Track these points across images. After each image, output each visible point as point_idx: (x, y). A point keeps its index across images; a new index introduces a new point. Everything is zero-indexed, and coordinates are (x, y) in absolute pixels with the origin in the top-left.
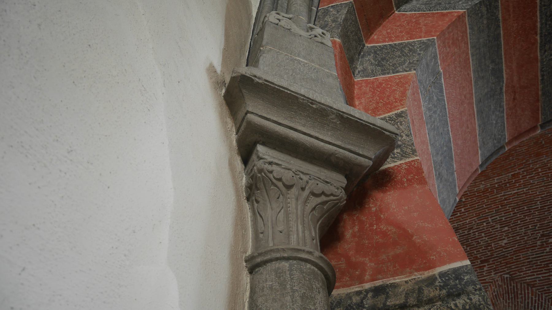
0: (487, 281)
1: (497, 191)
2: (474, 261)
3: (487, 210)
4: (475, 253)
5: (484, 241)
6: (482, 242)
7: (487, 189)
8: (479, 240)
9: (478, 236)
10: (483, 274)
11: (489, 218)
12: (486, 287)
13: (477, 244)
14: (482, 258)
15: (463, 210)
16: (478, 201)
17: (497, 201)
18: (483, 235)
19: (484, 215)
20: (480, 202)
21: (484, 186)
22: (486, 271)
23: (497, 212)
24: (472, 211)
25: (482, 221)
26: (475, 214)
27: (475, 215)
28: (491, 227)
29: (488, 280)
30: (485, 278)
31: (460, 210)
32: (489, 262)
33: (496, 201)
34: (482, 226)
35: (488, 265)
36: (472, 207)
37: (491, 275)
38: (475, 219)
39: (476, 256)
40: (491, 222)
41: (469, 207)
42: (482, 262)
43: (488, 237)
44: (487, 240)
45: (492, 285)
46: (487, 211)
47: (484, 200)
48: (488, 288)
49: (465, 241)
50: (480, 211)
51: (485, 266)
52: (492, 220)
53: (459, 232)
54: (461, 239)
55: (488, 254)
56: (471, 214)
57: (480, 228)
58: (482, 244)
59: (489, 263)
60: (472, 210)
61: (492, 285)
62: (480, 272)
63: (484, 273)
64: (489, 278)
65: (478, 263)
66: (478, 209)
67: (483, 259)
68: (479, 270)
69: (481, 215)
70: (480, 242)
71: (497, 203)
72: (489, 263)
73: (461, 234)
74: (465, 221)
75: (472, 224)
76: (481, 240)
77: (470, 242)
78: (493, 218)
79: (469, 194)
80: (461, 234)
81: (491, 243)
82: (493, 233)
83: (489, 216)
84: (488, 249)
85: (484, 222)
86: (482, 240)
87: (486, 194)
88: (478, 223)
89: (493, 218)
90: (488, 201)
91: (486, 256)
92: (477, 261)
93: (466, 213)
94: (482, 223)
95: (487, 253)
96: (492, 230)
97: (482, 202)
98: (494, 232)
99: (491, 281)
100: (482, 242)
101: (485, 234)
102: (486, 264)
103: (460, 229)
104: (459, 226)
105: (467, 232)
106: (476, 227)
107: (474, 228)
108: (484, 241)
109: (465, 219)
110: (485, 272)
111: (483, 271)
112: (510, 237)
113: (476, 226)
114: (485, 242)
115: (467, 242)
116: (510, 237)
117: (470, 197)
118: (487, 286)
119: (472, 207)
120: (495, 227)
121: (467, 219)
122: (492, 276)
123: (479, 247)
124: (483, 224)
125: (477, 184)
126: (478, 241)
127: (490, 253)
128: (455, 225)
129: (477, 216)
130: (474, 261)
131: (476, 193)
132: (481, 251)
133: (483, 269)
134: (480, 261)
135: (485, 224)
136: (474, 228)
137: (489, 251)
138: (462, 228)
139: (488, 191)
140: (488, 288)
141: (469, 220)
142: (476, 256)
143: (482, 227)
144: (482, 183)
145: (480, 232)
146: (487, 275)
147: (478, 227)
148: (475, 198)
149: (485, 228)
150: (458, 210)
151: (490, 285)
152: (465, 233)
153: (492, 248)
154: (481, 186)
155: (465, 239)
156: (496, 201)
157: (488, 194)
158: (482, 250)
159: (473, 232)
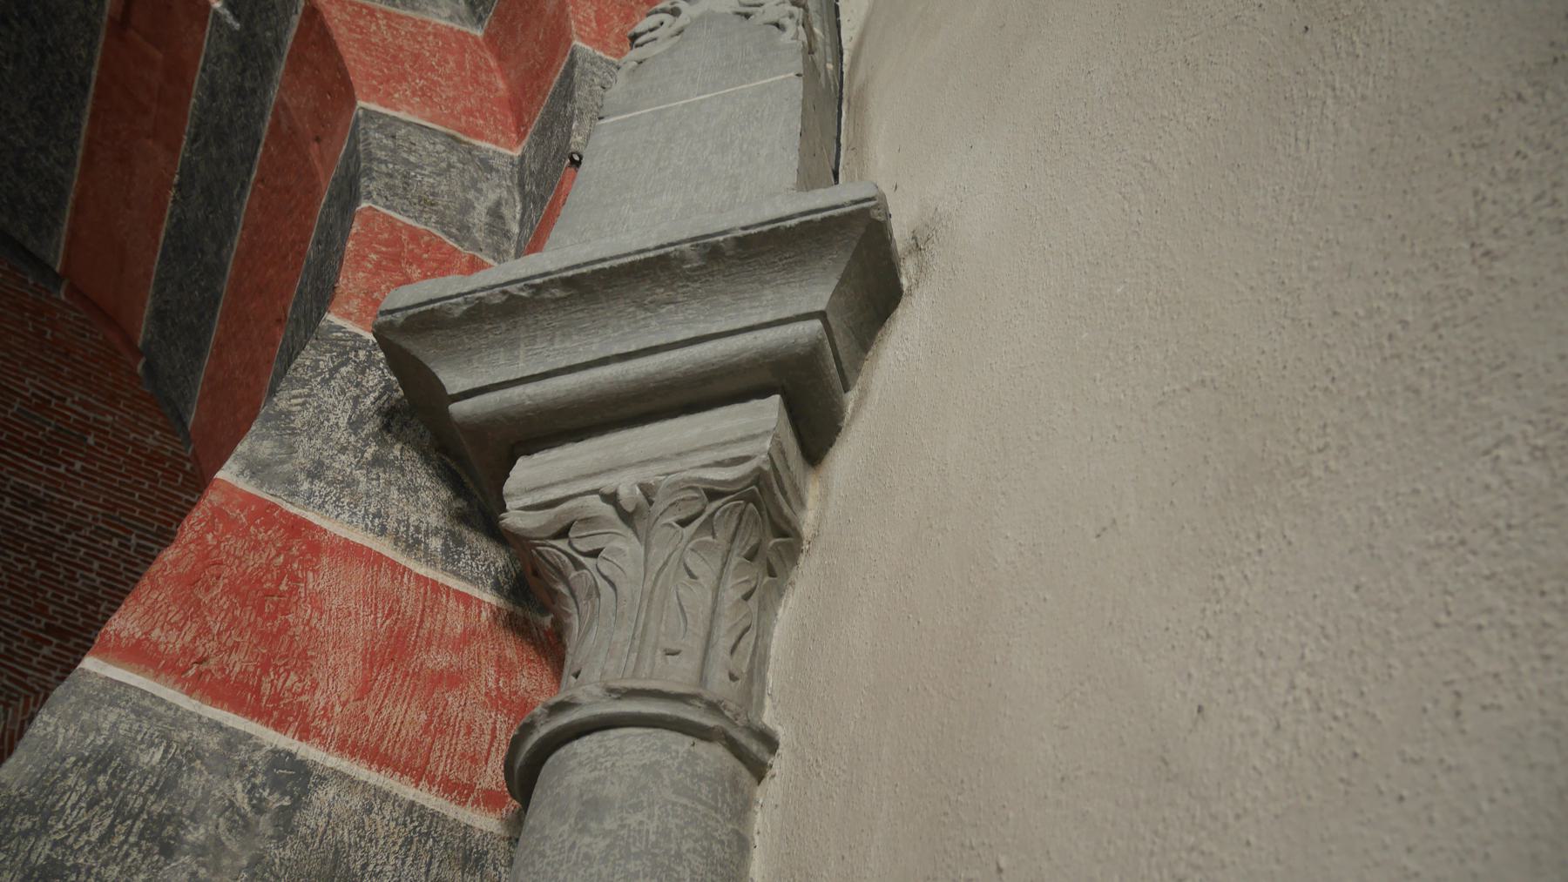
0: (28, 682)
1: (186, 483)
2: (32, 615)
3: (138, 510)
4: (49, 596)
5: (88, 582)
6: (81, 581)
7: (162, 459)
8: (80, 572)
9: (81, 559)
10: (31, 660)
11: (133, 537)
12: (16, 695)
13: (65, 577)
14: (56, 619)
15: (78, 465)
16: (126, 470)
17: (174, 508)
18: (96, 565)
19: (123, 519)
20: (129, 478)
21: (157, 443)
22: (44, 657)
23: (159, 533)
24: (100, 487)
25: (113, 530)
26: (105, 500)
27: (101, 501)
28: (125, 561)
29: (33, 682)
30: (30, 672)
31: (72, 460)
32: (68, 641)
33: (170, 506)
34: (107, 542)
35: (58, 646)
36: (106, 477)
37: (49, 674)
38: (96, 512)
39: (45, 603)
40: (132, 549)
41: (96, 469)
42: (49, 629)
43: (104, 580)
44: (97, 584)
45: (32, 700)
46: (137, 515)
47: (142, 480)
48: (17, 700)
49: (42, 549)
50: (119, 502)
51: (49, 643)
52: (139, 545)
53: (40, 515)
54: (36, 536)
55: (77, 620)
56: (96, 493)
57: (97, 542)
58: (78, 585)
59: (63, 643)
60: (102, 484)
61: (32, 700)
62: (26, 650)
63: (35, 659)
64: (39, 678)
65: (37, 626)
66: (118, 494)
67: (58, 623)
68: (29, 643)
69: (117, 514)
70: (78, 576)
71: (171, 513)
72: (63, 643)
73: (41, 522)
74: (69, 499)
75: (84, 519)
76: (83, 576)
77: (54, 560)
78: (143, 542)
79: (110, 437)
80: (41, 522)
81: (103, 599)
82: (122, 578)
83: (136, 531)
84: (86, 608)
85: (117, 536)
86: (87, 578)
87: (156, 471)
88: (100, 528)
89: (143, 542)
90: (152, 490)
91: (71, 621)
92: (39, 617)
93: (83, 481)
94: (108, 535)
95: (78, 616)
96: (125, 569)
97: (136, 481)
98: (127, 577)
99: (37, 688)
100: (81, 581)
101: (101, 567)
102: (55, 641)
103: (45, 509)
104: (48, 499)
105: (62, 531)
106: (88, 534)
107: (82, 533)
108: (88, 582)
109: (72, 493)
110: (40, 659)
111: (36, 650)
112: (58, 398)
113: (91, 532)
114: (88, 586)
115: (45, 554)
116: (58, 398)
117: (112, 447)
118: (20, 694)
119: (106, 477)
120: (136, 569)
121: (77, 499)
122: (48, 678)
123: (66, 588)
124: (110, 540)
125: (140, 424)
126: (74, 573)
127: (84, 623)
128: (38, 491)
129: (107, 508)
130: (32, 615)
131: (131, 448)
132: (65, 602)
133: (40, 648)
134: (47, 625)
135: (115, 543)
136: (82, 533)
137: (84, 615)
138: (53, 512)
139: (161, 465)
140: (17, 700)
141: (81, 503)
142: (45, 603)
143: (104, 545)
144: (153, 433)
145: (92, 552)
146: (39, 667)
147: (94, 537)
148: (122, 459)
149: (111, 552)
150: (67, 458)
151: (27, 697)
152: (53, 527)
153: (97, 613)
154: (150, 440)
155: (44, 542)
156: (170, 506)
157: (160, 473)
158: (70, 601)
159: (75, 542)
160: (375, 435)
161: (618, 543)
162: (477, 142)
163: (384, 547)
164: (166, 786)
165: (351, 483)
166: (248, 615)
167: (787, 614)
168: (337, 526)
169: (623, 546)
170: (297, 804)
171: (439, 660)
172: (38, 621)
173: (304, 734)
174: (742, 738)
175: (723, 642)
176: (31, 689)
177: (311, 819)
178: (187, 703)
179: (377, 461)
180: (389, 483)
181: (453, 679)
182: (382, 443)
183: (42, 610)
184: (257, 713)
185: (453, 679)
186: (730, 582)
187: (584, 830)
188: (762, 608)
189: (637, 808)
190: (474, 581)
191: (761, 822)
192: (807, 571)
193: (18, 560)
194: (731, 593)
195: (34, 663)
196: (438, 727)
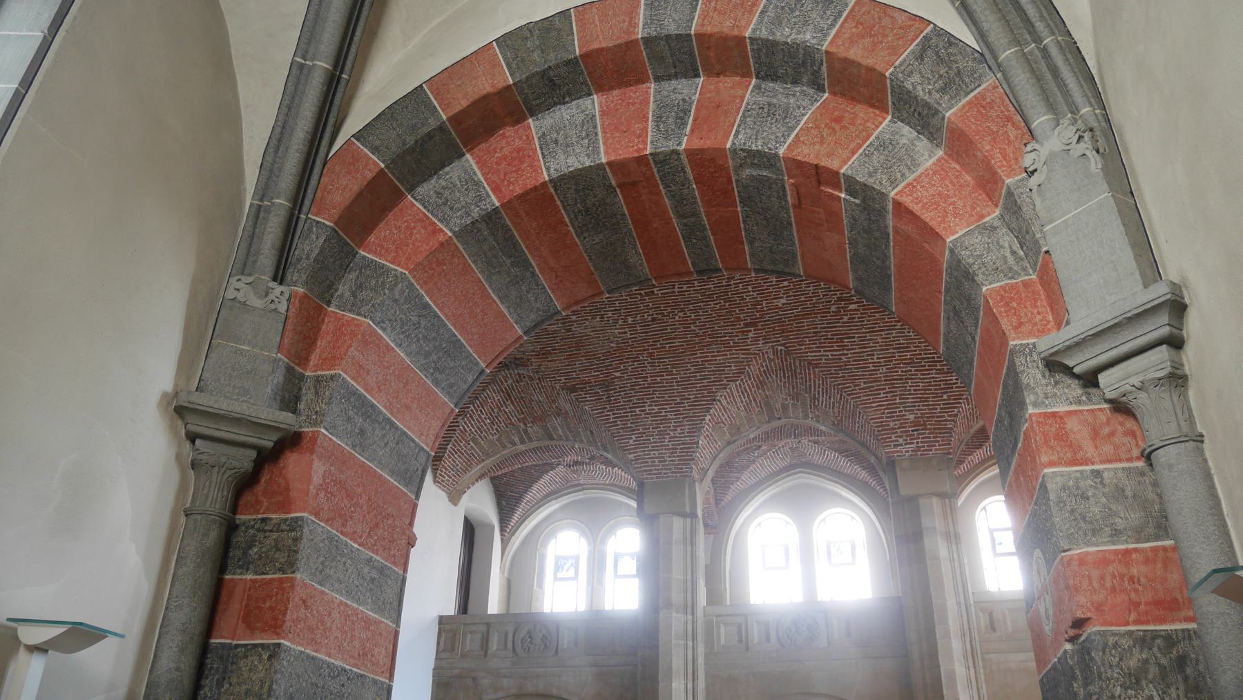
8: (744, 295)
18: (750, 288)
35: (755, 330)
42: (746, 325)
44: (756, 296)
51: (750, 331)
67: (749, 321)
101: (753, 288)
137: (757, 312)
151: (755, 358)
159: (735, 284)
160: (1049, 375)
161: (1140, 396)
162: (984, 221)
163: (1074, 407)
164: (1078, 488)
165: (1055, 394)
166: (1063, 443)
167: (1191, 393)
168: (1062, 408)
169: (1142, 396)
170: (1102, 480)
171: (1106, 430)
172: (740, 325)
173: (1093, 464)
174: (1195, 438)
175: (1180, 413)
176: (755, 354)
177: (1107, 481)
178: (1068, 469)
179: (1057, 383)
180: (1063, 388)
181: (1112, 434)
182: (1053, 377)
183: (739, 319)
184: (1081, 464)
185: (1112, 434)
186: (1173, 395)
187: (1171, 472)
188: (1184, 396)
189: (1180, 464)
190: (1099, 403)
191: (1208, 454)
192: (1192, 384)
193: (715, 304)
194: (1175, 398)
195: (749, 343)
196: (1117, 448)
